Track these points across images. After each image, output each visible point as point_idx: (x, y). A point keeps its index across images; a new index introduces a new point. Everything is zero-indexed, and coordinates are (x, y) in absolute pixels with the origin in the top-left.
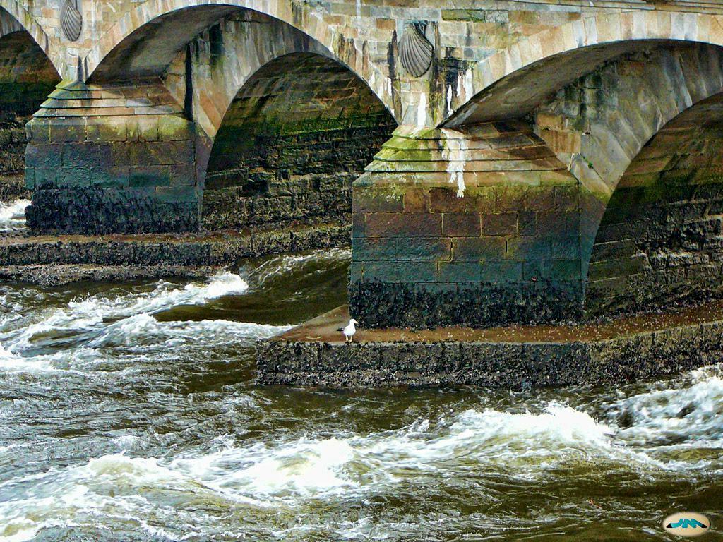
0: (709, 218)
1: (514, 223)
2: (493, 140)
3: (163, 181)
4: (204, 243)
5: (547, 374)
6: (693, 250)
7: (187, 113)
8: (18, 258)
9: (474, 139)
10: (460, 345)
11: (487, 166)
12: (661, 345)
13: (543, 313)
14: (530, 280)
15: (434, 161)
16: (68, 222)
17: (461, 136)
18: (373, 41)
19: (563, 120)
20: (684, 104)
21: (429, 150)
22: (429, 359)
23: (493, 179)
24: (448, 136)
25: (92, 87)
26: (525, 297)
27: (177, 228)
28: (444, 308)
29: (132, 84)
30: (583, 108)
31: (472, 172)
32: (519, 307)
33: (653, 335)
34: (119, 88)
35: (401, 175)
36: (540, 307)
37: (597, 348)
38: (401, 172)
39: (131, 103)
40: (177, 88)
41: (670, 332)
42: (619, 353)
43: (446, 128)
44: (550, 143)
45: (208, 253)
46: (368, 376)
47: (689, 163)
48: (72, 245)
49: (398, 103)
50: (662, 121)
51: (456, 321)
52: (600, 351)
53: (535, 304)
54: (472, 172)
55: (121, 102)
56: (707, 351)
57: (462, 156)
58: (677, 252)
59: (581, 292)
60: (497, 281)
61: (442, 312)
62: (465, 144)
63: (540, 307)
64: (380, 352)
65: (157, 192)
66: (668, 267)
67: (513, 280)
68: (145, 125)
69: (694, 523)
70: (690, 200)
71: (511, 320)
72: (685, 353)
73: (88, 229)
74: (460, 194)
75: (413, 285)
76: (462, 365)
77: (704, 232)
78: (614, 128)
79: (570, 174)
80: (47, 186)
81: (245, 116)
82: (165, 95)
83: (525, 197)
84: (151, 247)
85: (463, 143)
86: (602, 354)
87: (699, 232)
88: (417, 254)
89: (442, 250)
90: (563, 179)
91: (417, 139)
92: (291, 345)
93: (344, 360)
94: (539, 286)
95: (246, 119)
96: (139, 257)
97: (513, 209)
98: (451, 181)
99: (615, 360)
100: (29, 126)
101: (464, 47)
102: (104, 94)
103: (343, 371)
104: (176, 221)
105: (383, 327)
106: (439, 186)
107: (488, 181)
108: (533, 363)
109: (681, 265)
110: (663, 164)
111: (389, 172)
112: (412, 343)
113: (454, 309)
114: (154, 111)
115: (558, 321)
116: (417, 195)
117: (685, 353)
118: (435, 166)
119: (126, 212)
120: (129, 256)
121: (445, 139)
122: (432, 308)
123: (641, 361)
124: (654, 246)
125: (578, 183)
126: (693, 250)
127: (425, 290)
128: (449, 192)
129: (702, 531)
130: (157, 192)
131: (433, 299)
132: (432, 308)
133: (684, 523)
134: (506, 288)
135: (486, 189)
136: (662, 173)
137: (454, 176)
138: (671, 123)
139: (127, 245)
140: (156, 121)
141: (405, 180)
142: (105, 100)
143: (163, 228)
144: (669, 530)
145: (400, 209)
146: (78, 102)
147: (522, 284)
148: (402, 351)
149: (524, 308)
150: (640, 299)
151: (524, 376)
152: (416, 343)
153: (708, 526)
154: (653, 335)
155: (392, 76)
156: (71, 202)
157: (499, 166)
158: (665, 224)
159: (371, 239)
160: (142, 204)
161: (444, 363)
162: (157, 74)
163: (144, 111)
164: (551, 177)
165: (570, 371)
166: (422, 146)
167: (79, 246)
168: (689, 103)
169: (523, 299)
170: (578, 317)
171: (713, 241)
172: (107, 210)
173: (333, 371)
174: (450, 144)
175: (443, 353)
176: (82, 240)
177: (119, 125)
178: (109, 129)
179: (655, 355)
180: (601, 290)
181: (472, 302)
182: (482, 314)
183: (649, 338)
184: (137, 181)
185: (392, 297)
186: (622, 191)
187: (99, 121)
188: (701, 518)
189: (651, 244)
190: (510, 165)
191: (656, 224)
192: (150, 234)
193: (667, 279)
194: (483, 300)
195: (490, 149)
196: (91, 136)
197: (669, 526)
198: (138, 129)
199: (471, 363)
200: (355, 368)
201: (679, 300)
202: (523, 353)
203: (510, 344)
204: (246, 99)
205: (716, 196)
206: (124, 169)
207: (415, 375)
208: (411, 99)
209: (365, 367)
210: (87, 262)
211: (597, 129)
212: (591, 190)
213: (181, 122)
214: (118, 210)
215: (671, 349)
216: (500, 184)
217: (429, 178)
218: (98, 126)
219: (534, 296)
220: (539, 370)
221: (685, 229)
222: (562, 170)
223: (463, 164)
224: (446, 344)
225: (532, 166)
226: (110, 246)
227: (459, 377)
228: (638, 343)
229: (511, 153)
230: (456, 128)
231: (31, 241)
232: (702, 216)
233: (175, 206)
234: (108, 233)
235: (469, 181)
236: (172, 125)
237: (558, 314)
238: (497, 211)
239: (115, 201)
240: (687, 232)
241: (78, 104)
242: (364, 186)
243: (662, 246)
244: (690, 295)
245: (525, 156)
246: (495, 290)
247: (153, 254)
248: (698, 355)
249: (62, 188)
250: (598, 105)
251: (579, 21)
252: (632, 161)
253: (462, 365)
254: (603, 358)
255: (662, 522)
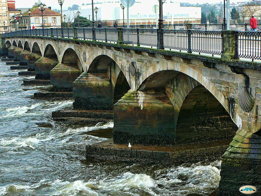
0: (214, 117)
1: (156, 117)
2: (152, 94)
3: (104, 97)
4: (111, 114)
5: (158, 160)
6: (210, 126)
7: (110, 81)
8: (68, 115)
9: (147, 94)
10: (136, 151)
11: (149, 101)
12: (193, 154)
13: (164, 142)
14: (160, 133)
15: (135, 100)
16: (82, 106)
17: (143, 93)
18: (126, 66)
19: (171, 89)
20: (193, 88)
21: (134, 96)
22: (128, 154)
23: (151, 105)
24: (139, 93)
25: (89, 74)
26: (159, 137)
27: (108, 109)
28: (137, 139)
29: (99, 73)
30: (174, 87)
31: (145, 103)
32: (157, 140)
33: (191, 151)
34: (95, 74)
35: (126, 103)
36: (163, 141)
37: (172, 154)
38: (126, 102)
39: (97, 78)
40: (109, 74)
41: (196, 150)
42: (179, 155)
43: (139, 91)
44: (169, 96)
45: (112, 116)
46: (111, 158)
47: (203, 103)
48: (81, 112)
49: (130, 83)
50: (189, 92)
51: (141, 143)
52: (173, 155)
53: (162, 139)
54: (145, 103)
55: (95, 77)
56: (208, 156)
57: (143, 98)
58: (205, 127)
59: (174, 137)
60: (151, 133)
61: (137, 140)
62: (144, 95)
63: (163, 141)
64: (116, 151)
65: (103, 100)
66: (202, 131)
67: (156, 133)
68: (100, 83)
69: (250, 189)
70: (206, 112)
71: (155, 144)
72: (201, 156)
73: (87, 109)
74: (142, 109)
75: (129, 133)
76: (137, 156)
77: (213, 121)
78: (180, 93)
79: (172, 104)
80: (78, 98)
81: (122, 82)
82: (106, 76)
83: (159, 110)
84: (99, 114)
85: (143, 95)
86: (174, 156)
87: (211, 121)
88: (130, 124)
89: (137, 124)
90: (170, 106)
91: (131, 93)
92: (94, 147)
93: (107, 153)
94: (163, 135)
95: (122, 83)
96: (96, 116)
97: (156, 113)
98: (139, 105)
99: (178, 158)
100: (74, 83)
101: (140, 69)
102: (91, 75)
103: (106, 155)
104: (108, 107)
105: (121, 144)
106: (136, 106)
107: (149, 105)
108: (155, 157)
109: (206, 130)
110: (194, 103)
111: (123, 102)
112: (124, 149)
113: (140, 140)
114: (103, 80)
115: (168, 145)
116: (130, 108)
117: (201, 156)
118: (135, 101)
119: (96, 105)
120: (93, 116)
121: (139, 94)
122: (134, 139)
123: (187, 158)
124: (197, 125)
125: (173, 107)
126: (210, 126)
127: (132, 135)
128: (139, 108)
129: (254, 192)
130: (103, 100)
131: (135, 137)
132: (134, 139)
133: (247, 189)
134: (154, 135)
135: (149, 108)
136: (195, 105)
137: (140, 104)
138: (190, 92)
139: (93, 113)
140: (103, 82)
141: (127, 104)
142: (91, 77)
143: (105, 109)
144: (242, 192)
145: (126, 112)
146: (85, 77)
147: (158, 134)
148: (121, 151)
149: (159, 141)
150: (193, 139)
151: (152, 160)
152: (125, 149)
153: (256, 190)
154: (191, 151)
155: (129, 76)
156: (83, 102)
157: (152, 101)
158: (200, 119)
159: (119, 120)
160: (99, 103)
161: (132, 155)
162: (105, 70)
163: (100, 80)
164: (166, 105)
165: (165, 160)
166: (132, 95)
167: (82, 113)
168: (194, 88)
169: (159, 138)
170: (173, 144)
171: (216, 124)
172: (91, 104)
173: (104, 155)
174: (140, 95)
175: (132, 153)
176: (85, 111)
177: (94, 83)
178: (92, 84)
179: (191, 157)
180: (180, 137)
181: (145, 138)
182: (148, 142)
183: (189, 152)
184: (98, 97)
185: (124, 136)
186: (182, 109)
187: (90, 82)
188: (253, 188)
189: (196, 124)
190: (155, 101)
191: (197, 119)
192: (101, 110)
193: (202, 134)
194: (148, 138)
195: (150, 97)
196: (88, 86)
197: (242, 190)
198: (98, 84)
199: (139, 156)
200: (110, 155)
201: (207, 140)
202: (152, 154)
203: (149, 151)
204: (121, 78)
205: (215, 111)
206: (95, 94)
207: (124, 158)
208: (132, 82)
209: (112, 155)
210: (84, 117)
211: (176, 92)
212: (176, 109)
213: (108, 83)
214: (94, 104)
215: (196, 155)
216: (152, 107)
217: (133, 104)
218: (89, 83)
219: (161, 137)
220: (156, 159)
221: (207, 120)
222: (170, 103)
223: (143, 100)
224: (133, 150)
225: (161, 102)
226: (89, 113)
227: (135, 160)
228: (186, 153)
229: (156, 98)
230: (141, 91)
231: (73, 111)
232: (212, 117)
233: (107, 104)
234: (92, 110)
235: (144, 105)
236: (106, 83)
237: (168, 143)
238: (151, 114)
239: (93, 102)
240: (207, 121)
241: (85, 78)
242: (117, 105)
243: (200, 125)
244: (210, 138)
245: (159, 99)
246: (151, 135)
247: (99, 116)
248: (205, 157)
249: (81, 98)
250: (177, 86)
251: (159, 64)
252: (183, 102)
253: (137, 156)
254: (174, 157)
255: (239, 189)
